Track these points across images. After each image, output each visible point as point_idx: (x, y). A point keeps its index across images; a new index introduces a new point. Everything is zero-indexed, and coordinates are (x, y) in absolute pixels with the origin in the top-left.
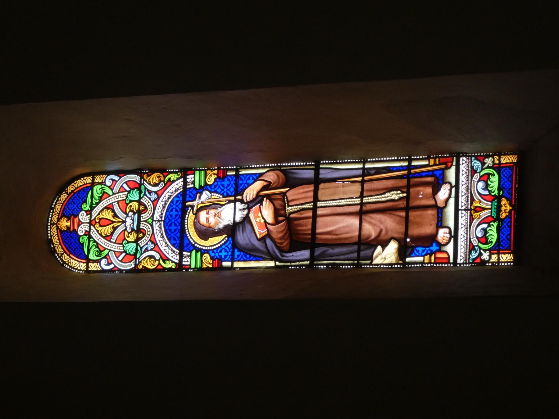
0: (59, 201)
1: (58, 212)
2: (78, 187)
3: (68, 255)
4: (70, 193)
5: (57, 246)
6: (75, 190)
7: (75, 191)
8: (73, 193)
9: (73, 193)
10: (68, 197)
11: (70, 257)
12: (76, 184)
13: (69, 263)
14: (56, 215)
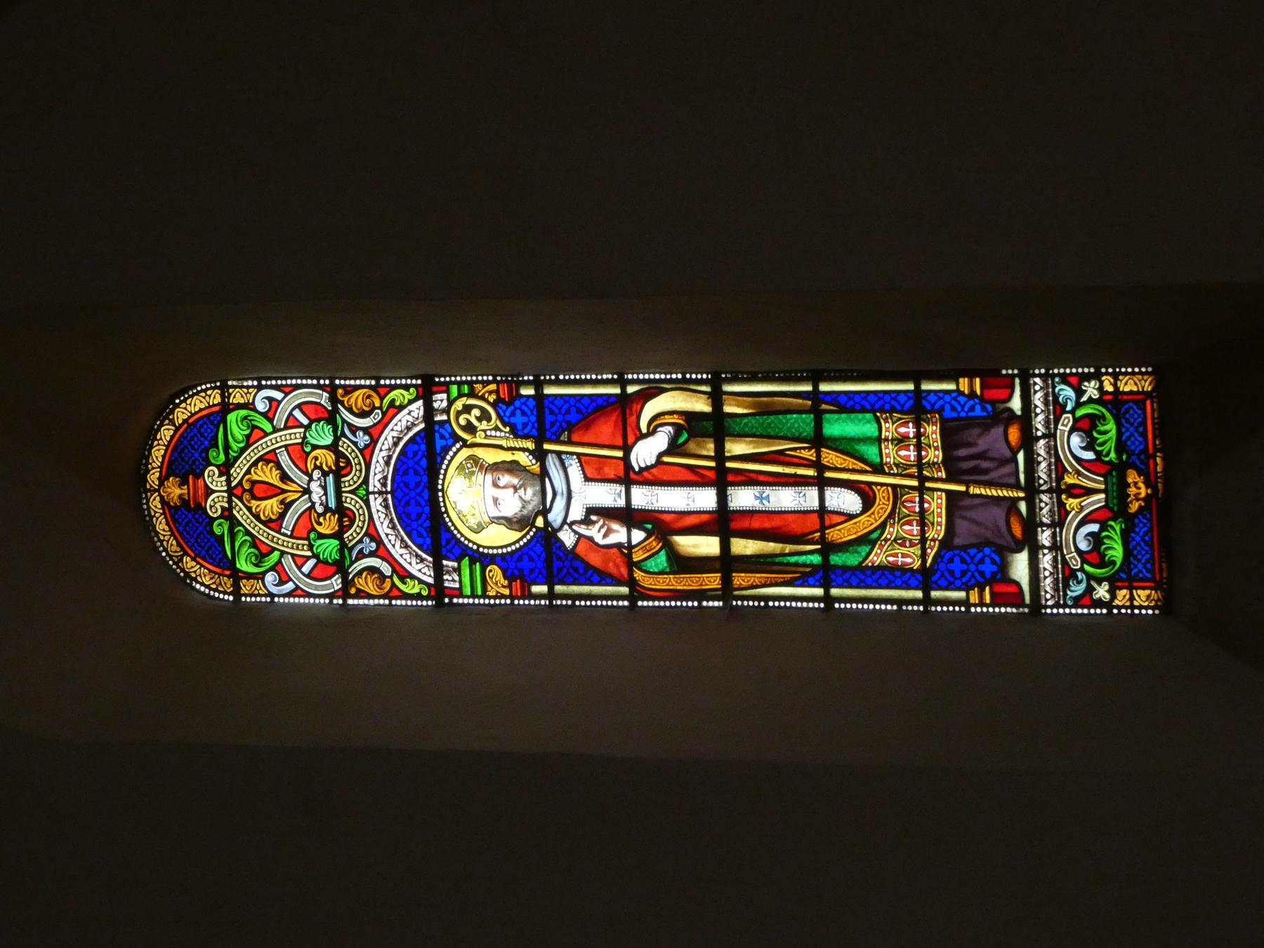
0: (158, 440)
1: (161, 511)
2: (196, 413)
3: (193, 559)
4: (181, 425)
5: (166, 538)
6: (189, 418)
7: (190, 421)
8: (186, 425)
9: (186, 425)
10: (175, 432)
11: (198, 563)
12: (190, 404)
13: (197, 576)
14: (160, 519)
